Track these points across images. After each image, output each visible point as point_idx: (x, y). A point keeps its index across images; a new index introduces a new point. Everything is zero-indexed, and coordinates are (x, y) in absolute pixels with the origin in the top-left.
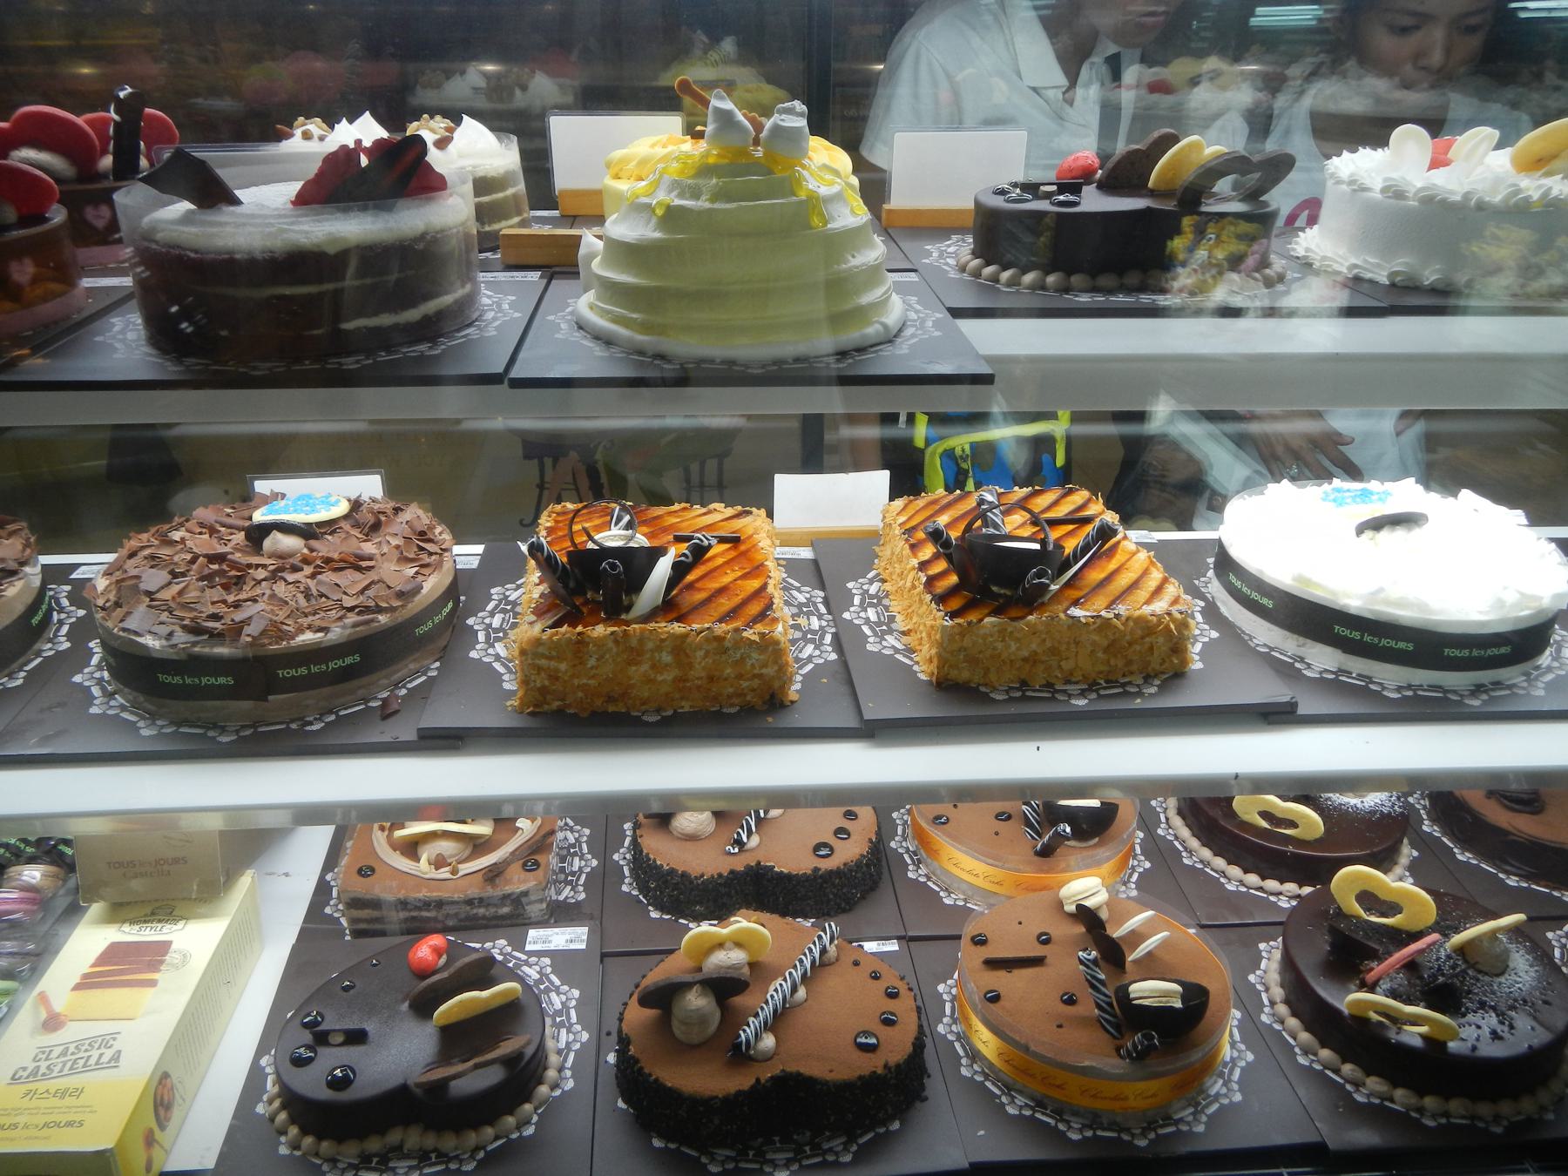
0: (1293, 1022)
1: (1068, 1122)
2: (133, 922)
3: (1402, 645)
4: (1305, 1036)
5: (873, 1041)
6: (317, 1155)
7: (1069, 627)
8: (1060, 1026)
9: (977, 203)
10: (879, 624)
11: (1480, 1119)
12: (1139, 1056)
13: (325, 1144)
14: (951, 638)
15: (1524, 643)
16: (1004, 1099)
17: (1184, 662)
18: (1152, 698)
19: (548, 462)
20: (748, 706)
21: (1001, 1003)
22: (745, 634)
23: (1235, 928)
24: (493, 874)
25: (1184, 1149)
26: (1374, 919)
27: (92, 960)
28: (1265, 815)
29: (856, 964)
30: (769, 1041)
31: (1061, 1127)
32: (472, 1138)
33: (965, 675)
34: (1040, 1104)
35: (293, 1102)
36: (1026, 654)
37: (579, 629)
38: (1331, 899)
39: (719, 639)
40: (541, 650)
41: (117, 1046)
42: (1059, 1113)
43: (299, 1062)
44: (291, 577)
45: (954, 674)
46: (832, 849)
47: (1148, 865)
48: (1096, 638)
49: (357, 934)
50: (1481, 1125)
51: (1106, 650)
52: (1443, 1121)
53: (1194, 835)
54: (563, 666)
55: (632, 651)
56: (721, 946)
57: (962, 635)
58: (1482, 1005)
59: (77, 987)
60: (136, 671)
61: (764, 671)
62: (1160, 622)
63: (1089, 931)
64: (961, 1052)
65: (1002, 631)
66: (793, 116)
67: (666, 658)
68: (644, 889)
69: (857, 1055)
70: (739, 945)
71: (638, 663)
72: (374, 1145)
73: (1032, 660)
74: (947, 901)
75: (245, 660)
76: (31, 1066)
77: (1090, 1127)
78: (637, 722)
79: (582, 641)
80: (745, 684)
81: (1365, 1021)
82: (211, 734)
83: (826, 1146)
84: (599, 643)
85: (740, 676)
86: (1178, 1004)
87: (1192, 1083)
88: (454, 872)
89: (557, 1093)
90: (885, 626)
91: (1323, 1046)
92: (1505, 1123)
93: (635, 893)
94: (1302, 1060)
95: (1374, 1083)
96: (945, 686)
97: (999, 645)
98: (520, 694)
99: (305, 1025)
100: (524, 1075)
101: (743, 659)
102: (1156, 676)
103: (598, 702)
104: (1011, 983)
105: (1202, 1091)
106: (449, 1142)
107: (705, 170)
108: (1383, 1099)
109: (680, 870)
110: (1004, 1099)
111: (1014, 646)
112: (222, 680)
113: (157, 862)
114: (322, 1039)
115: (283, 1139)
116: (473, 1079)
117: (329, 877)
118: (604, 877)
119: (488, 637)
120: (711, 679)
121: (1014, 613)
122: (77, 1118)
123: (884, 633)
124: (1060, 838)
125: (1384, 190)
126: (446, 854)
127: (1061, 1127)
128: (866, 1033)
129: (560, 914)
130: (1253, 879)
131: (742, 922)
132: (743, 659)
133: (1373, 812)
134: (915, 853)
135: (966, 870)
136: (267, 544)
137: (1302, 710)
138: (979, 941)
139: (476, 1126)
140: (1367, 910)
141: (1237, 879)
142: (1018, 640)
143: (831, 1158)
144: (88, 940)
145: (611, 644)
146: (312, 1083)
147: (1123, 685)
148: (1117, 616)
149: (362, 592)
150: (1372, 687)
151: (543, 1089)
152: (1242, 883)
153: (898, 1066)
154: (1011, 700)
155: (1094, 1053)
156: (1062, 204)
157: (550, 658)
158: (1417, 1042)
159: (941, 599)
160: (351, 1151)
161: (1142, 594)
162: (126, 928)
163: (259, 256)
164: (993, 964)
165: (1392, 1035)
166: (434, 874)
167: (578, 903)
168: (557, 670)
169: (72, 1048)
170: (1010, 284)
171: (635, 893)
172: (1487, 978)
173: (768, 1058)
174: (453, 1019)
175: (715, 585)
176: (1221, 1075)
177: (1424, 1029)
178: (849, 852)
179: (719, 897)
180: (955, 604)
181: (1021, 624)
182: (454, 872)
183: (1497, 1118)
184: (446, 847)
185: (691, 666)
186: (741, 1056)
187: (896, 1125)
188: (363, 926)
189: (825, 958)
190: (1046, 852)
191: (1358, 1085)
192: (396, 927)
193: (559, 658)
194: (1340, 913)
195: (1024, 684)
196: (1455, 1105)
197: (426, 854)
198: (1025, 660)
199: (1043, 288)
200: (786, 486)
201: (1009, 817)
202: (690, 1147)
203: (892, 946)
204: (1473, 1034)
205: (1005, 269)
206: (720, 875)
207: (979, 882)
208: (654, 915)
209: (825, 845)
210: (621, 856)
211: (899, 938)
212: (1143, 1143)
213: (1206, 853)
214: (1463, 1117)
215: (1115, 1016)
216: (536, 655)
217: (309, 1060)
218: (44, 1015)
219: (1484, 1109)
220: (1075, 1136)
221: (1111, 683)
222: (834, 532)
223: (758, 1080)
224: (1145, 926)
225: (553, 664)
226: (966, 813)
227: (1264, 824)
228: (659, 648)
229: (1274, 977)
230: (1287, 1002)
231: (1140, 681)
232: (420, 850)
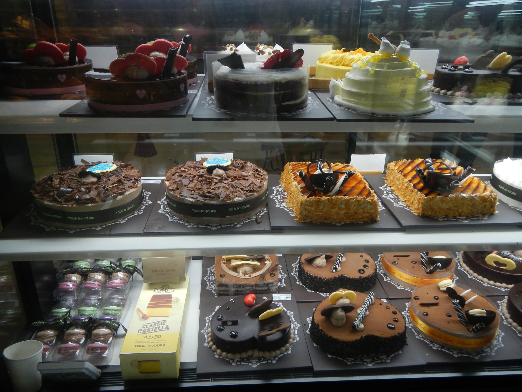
0: (515, 324)
1: (452, 352)
2: (158, 289)
6: (227, 358)
10: (281, 199)
12: (477, 331)
13: (229, 355)
14: (427, 202)
16: (431, 345)
17: (494, 211)
18: (486, 221)
19: (269, 151)
20: (366, 222)
24: (262, 276)
25: (488, 360)
27: (150, 300)
29: (381, 304)
30: (362, 326)
31: (451, 353)
32: (274, 354)
33: (430, 213)
35: (218, 342)
36: (448, 207)
37: (318, 197)
39: (359, 201)
40: (307, 203)
41: (167, 324)
42: (449, 349)
43: (220, 330)
44: (226, 182)
45: (426, 213)
47: (458, 278)
48: (469, 202)
49: (219, 295)
51: (471, 206)
54: (313, 209)
55: (333, 204)
56: (341, 298)
57: (430, 201)
59: (148, 307)
60: (180, 208)
61: (371, 211)
62: (488, 198)
63: (449, 295)
64: (414, 331)
66: (405, 44)
67: (343, 206)
69: (389, 330)
70: (347, 298)
71: (335, 208)
72: (244, 355)
73: (450, 209)
74: (398, 288)
75: (221, 205)
76: (143, 329)
77: (460, 353)
78: (335, 226)
79: (319, 201)
80: (365, 215)
82: (186, 224)
83: (381, 358)
84: (324, 202)
85: (363, 213)
86: (485, 315)
87: (489, 340)
88: (250, 276)
89: (295, 341)
90: (398, 200)
93: (301, 284)
94: (519, 335)
96: (424, 216)
98: (299, 217)
99: (219, 320)
100: (286, 335)
101: (365, 208)
103: (323, 220)
104: (430, 310)
105: (491, 344)
106: (267, 355)
107: (382, 60)
110: (431, 345)
111: (444, 205)
112: (212, 211)
113: (167, 271)
114: (224, 323)
115: (215, 353)
116: (274, 336)
117: (205, 279)
118: (289, 279)
119: (277, 193)
120: (355, 213)
122: (162, 344)
123: (282, 202)
124: (437, 267)
126: (247, 271)
127: (451, 353)
128: (391, 324)
129: (280, 290)
130: (492, 282)
131: (341, 292)
132: (365, 208)
135: (403, 277)
136: (215, 172)
138: (416, 298)
139: (274, 350)
141: (486, 282)
142: (446, 203)
143: (384, 361)
144: (145, 295)
145: (327, 202)
146: (225, 335)
148: (476, 196)
149: (249, 186)
151: (291, 340)
152: (488, 284)
154: (445, 221)
155: (459, 330)
156: (467, 72)
157: (309, 206)
159: (421, 190)
160: (238, 357)
162: (156, 291)
163: (264, 83)
164: (423, 305)
166: (243, 277)
168: (311, 210)
169: (153, 325)
171: (301, 284)
173: (362, 331)
174: (264, 318)
176: (496, 339)
178: (368, 272)
179: (331, 285)
182: (250, 276)
184: (247, 269)
185: (350, 209)
186: (354, 329)
188: (221, 292)
190: (431, 272)
192: (232, 293)
193: (312, 206)
195: (447, 216)
197: (241, 270)
198: (447, 209)
201: (416, 263)
202: (340, 357)
206: (331, 278)
207: (409, 282)
208: (309, 291)
209: (362, 270)
210: (294, 274)
211: (386, 299)
212: (477, 358)
213: (475, 275)
215: (465, 319)
216: (305, 205)
217: (223, 330)
218: (141, 315)
220: (456, 356)
225: (310, 208)
227: (495, 265)
228: (341, 204)
229: (505, 311)
230: (511, 318)
231: (481, 216)
232: (238, 270)
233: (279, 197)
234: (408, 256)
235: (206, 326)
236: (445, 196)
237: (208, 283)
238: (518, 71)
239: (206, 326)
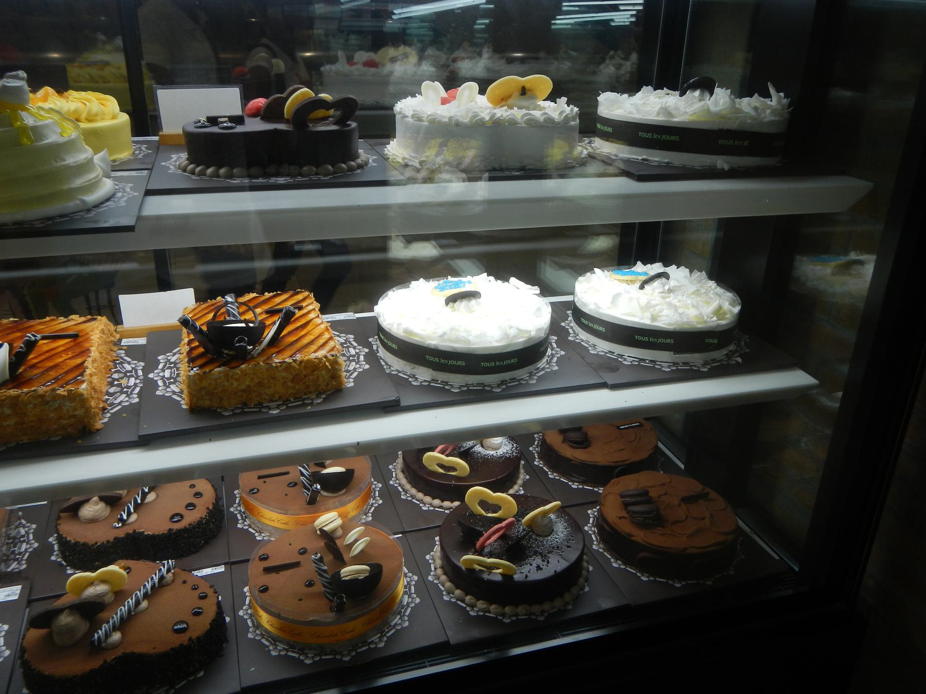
3: (459, 363)
4: (448, 584)
5: (185, 625)
7: (267, 370)
8: (300, 600)
9: (183, 129)
11: (534, 614)
15: (527, 355)
17: (341, 383)
21: (269, 592)
22: (58, 392)
23: (417, 532)
26: (490, 515)
28: (441, 466)
30: (116, 636)
33: (207, 403)
34: (292, 647)
36: (243, 387)
38: (467, 508)
39: (42, 396)
42: (302, 651)
45: (201, 403)
46: (182, 516)
50: (533, 617)
52: (514, 618)
53: (409, 482)
58: (536, 553)
61: (76, 413)
65: (226, 376)
68: (64, 558)
73: (248, 390)
81: (473, 570)
91: (457, 588)
92: (546, 614)
95: (481, 604)
96: (195, 410)
97: (226, 384)
102: (324, 392)
104: (272, 580)
108: (485, 612)
109: (82, 541)
110: (271, 648)
111: (235, 384)
121: (234, 364)
124: (317, 492)
125: (413, 116)
130: (437, 502)
133: (501, 457)
134: (244, 513)
137: (404, 403)
140: (487, 511)
142: (237, 380)
147: (303, 400)
148: (295, 361)
150: (487, 388)
152: (431, 505)
153: (198, 638)
154: (234, 415)
158: (499, 578)
161: (314, 347)
164: (268, 570)
165: (486, 576)
167: (20, 572)
170: (212, 176)
172: (541, 538)
173: (115, 646)
175: (51, 364)
177: (500, 571)
179: (88, 556)
180: (199, 362)
181: (237, 371)
183: (542, 612)
186: (97, 648)
187: (202, 674)
189: (164, 582)
191: (472, 606)
194: (473, 515)
196: (521, 609)
198: (242, 391)
199: (218, 176)
200: (129, 303)
201: (296, 484)
203: (221, 569)
204: (530, 571)
205: (198, 166)
207: (275, 524)
209: (177, 515)
211: (225, 564)
214: (525, 615)
219: (536, 609)
221: (296, 399)
222: (157, 328)
223: (105, 661)
224: (357, 539)
226: (275, 486)
227: (441, 471)
233: (353, 351)
234: (287, 473)
235: (409, 609)
236: (231, 368)
237: (239, 517)
238: (335, 124)
239: (409, 609)
